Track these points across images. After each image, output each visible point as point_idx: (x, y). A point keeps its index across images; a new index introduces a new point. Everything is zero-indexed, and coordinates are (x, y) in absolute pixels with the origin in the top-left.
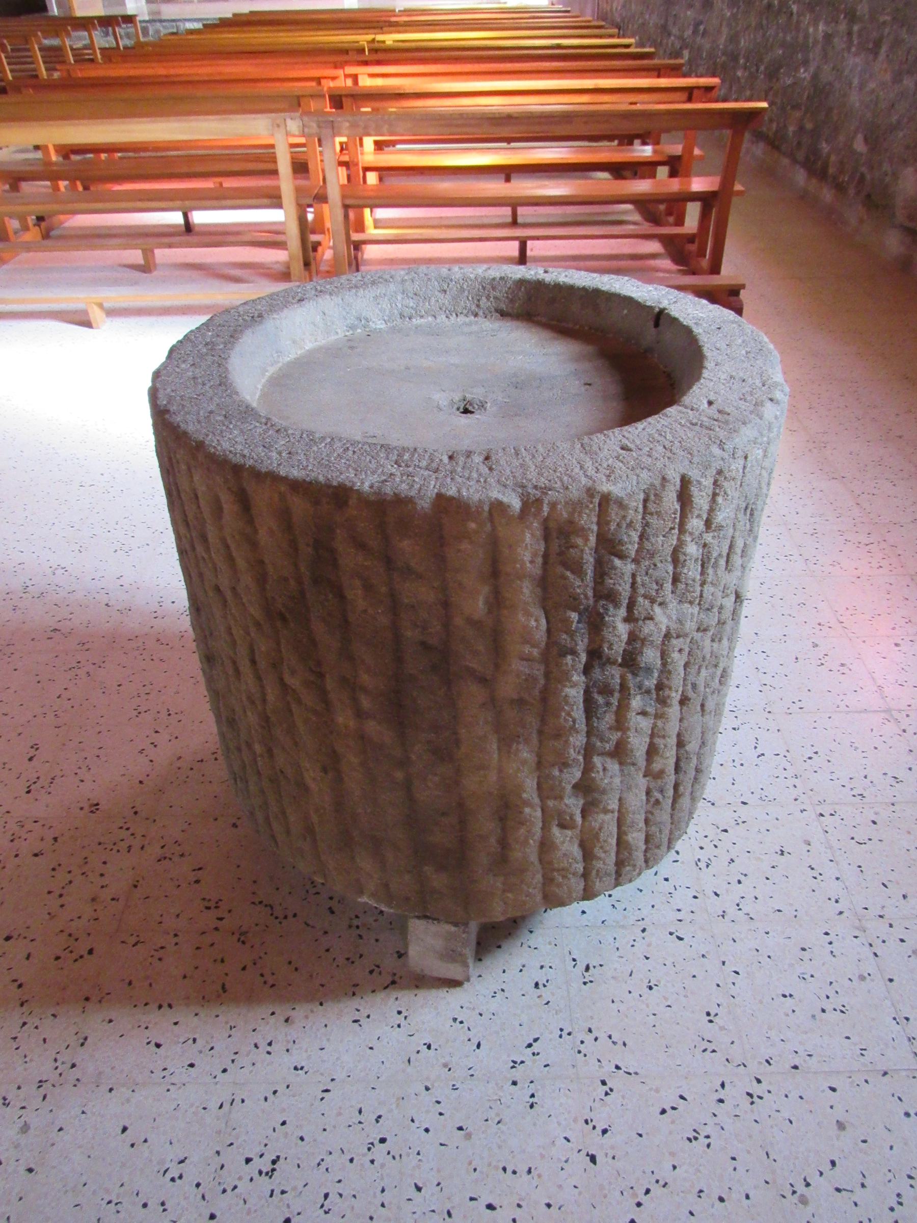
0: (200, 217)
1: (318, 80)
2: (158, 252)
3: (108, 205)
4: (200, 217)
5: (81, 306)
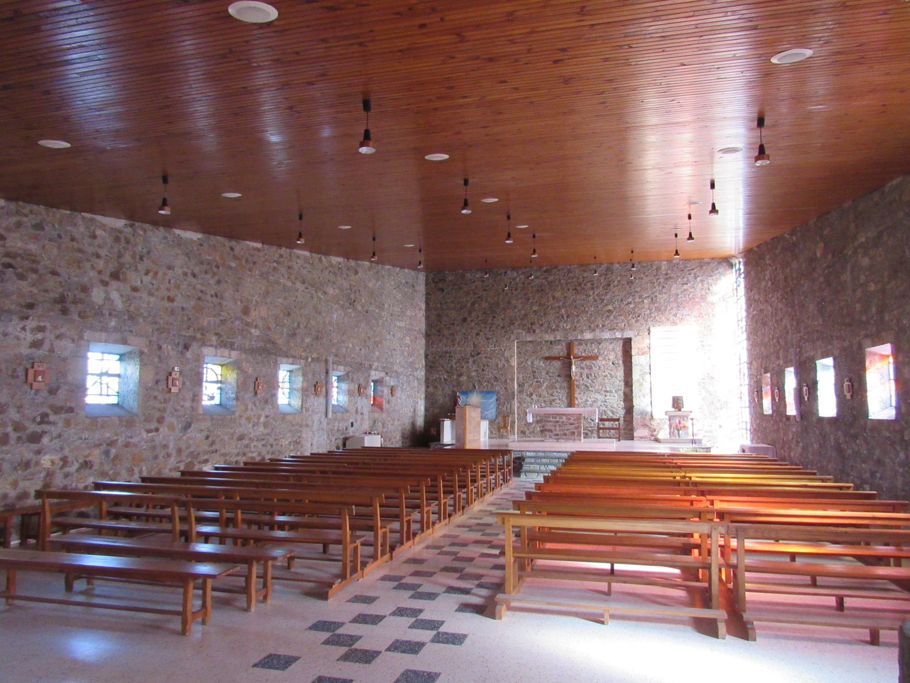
0: (617, 567)
1: (692, 502)
2: (613, 584)
3: (571, 557)
4: (617, 567)
5: (600, 611)
